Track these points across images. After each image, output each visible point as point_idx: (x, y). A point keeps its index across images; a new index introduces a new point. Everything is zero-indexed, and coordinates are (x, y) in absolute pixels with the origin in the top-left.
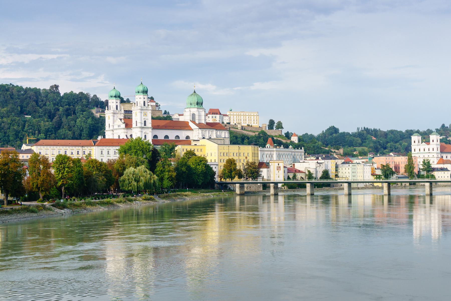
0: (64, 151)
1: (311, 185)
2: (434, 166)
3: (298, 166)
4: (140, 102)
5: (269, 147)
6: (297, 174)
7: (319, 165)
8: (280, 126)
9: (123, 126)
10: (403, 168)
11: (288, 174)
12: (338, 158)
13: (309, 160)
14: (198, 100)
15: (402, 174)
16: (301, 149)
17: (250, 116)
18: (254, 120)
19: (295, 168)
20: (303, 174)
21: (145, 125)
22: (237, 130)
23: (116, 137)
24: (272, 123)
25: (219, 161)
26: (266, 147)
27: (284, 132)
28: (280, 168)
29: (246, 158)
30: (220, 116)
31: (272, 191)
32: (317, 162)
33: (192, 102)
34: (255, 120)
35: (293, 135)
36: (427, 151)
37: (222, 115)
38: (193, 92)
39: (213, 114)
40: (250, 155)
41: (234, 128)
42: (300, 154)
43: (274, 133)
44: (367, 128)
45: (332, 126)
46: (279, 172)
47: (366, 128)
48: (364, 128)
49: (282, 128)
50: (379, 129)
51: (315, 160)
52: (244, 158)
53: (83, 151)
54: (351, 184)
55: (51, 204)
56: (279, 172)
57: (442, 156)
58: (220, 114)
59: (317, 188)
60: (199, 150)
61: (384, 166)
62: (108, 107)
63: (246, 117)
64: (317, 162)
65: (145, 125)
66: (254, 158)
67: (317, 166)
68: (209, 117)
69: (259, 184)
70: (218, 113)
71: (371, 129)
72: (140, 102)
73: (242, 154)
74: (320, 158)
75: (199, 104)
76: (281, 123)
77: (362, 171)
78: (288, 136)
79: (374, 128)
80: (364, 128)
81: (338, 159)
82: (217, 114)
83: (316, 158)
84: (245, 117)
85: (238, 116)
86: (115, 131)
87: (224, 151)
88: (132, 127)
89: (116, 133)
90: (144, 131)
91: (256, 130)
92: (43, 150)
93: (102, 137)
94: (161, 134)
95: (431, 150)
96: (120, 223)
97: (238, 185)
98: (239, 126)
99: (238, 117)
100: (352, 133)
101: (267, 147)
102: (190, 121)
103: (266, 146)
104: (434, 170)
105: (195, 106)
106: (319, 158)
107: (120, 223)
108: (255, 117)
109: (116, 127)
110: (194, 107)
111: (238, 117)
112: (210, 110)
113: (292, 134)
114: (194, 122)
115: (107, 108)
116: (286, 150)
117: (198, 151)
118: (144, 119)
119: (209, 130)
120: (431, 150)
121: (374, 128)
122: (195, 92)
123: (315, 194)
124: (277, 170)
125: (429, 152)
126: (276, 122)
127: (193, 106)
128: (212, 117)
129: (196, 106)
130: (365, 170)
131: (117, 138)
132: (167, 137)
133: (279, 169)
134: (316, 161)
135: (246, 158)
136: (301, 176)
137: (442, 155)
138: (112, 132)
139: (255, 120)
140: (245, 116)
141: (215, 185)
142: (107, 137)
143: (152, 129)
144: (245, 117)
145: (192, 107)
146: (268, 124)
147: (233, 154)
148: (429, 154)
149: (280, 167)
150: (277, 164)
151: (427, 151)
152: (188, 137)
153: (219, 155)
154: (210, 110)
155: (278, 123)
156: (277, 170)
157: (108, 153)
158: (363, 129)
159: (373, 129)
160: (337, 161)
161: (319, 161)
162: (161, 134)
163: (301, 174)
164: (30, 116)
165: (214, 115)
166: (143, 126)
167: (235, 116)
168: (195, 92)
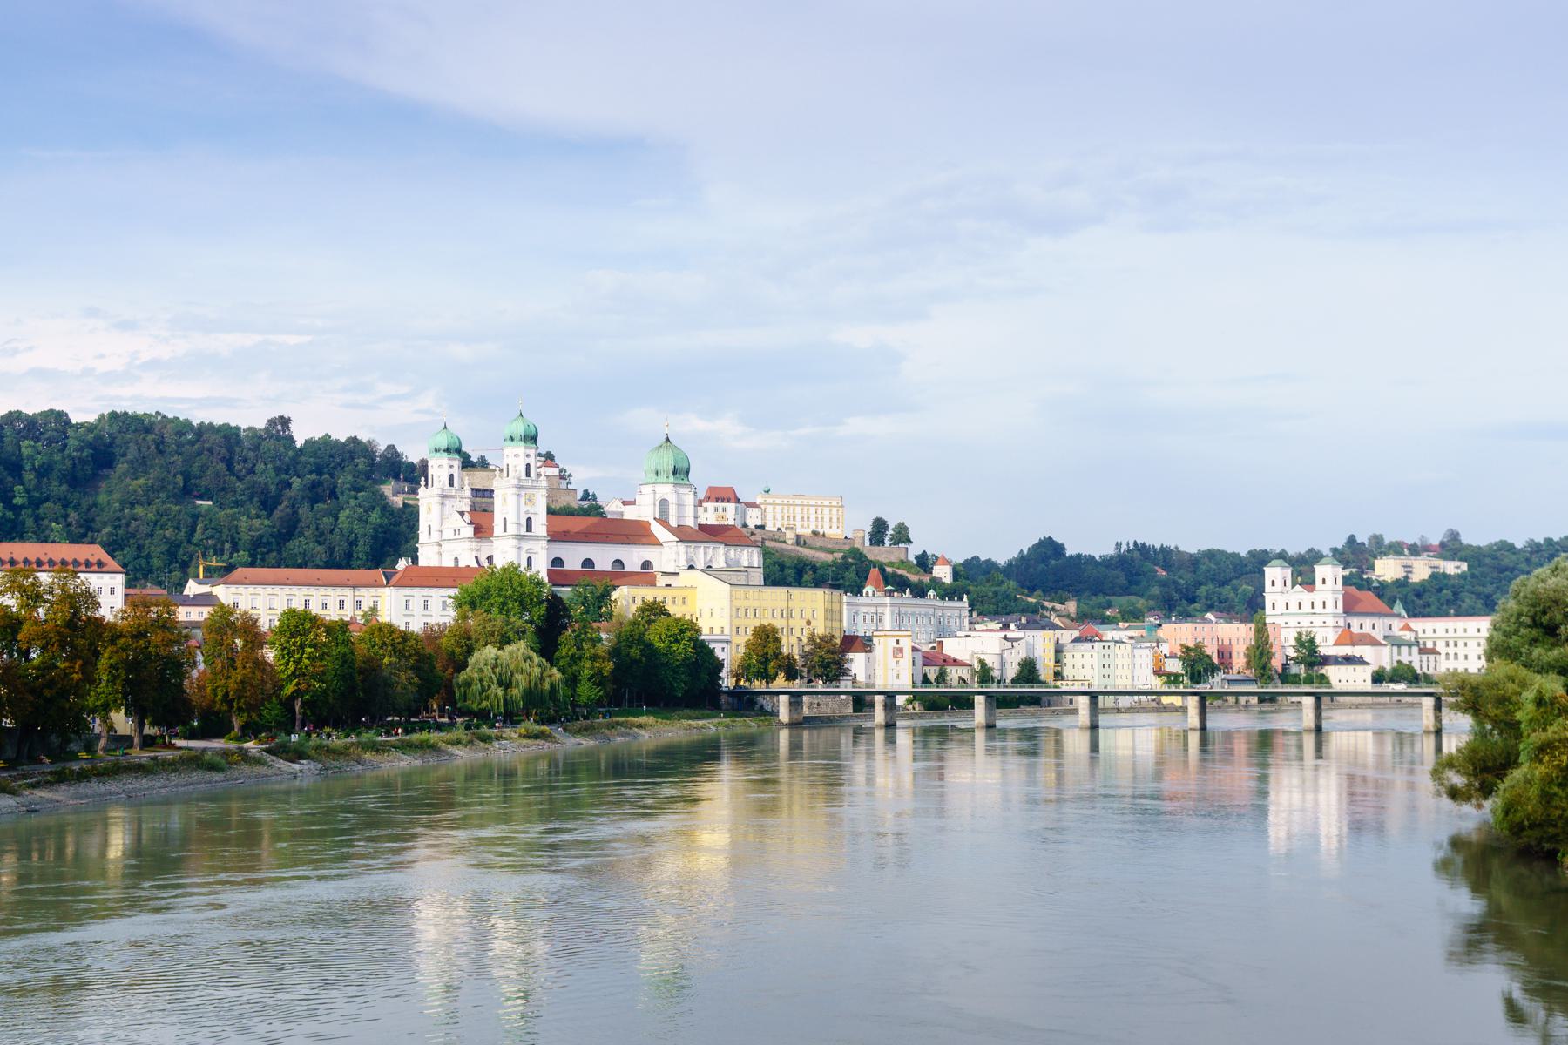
0: (304, 598)
1: (986, 701)
2: (1326, 649)
3: (952, 648)
5: (870, 594)
6: (949, 669)
7: (1009, 644)
8: (902, 536)
10: (1242, 655)
11: (925, 668)
12: (1061, 625)
13: (983, 631)
14: (676, 461)
15: (1239, 673)
16: (961, 599)
18: (831, 519)
20: (965, 669)
21: (529, 528)
22: (784, 546)
24: (879, 527)
27: (913, 552)
28: (902, 653)
29: (809, 623)
30: (736, 508)
31: (879, 715)
32: (1006, 636)
34: (835, 520)
35: (940, 561)
36: (1306, 608)
38: (664, 439)
39: (717, 500)
40: (820, 614)
41: (775, 540)
42: (957, 613)
43: (885, 554)
44: (1143, 545)
45: (1047, 537)
46: (898, 662)
47: (1139, 543)
48: (1135, 543)
49: (909, 541)
50: (1177, 548)
51: (998, 631)
52: (804, 623)
53: (356, 599)
54: (1097, 697)
56: (898, 662)
57: (1349, 624)
58: (738, 501)
59: (952, 709)
60: (679, 601)
61: (1188, 649)
62: (426, 480)
63: (808, 510)
64: (1006, 636)
65: (529, 528)
68: (706, 510)
69: (843, 697)
70: (732, 497)
71: (1154, 546)
73: (796, 613)
74: (1012, 626)
75: (680, 474)
76: (906, 529)
77: (1127, 661)
78: (924, 562)
79: (1162, 545)
80: (1135, 543)
81: (1061, 628)
83: (1001, 625)
85: (786, 507)
86: (445, 546)
87: (746, 604)
90: (526, 545)
94: (573, 555)
95: (1318, 608)
97: (784, 699)
98: (790, 536)
99: (786, 511)
100: (1101, 557)
101: (867, 593)
104: (1326, 660)
108: (834, 510)
109: (448, 534)
110: (665, 480)
111: (786, 511)
112: (711, 489)
113: (936, 560)
114: (663, 522)
115: (423, 483)
116: (919, 601)
117: (674, 602)
118: (527, 512)
120: (1318, 608)
121: (1162, 545)
124: (895, 657)
125: (1313, 611)
126: (892, 524)
127: (662, 478)
128: (716, 510)
129: (672, 479)
130: (1138, 661)
131: (452, 564)
132: (588, 563)
133: (900, 655)
134: (1002, 634)
135: (809, 623)
136: (960, 674)
137: (1349, 620)
138: (436, 548)
139: (835, 520)
142: (422, 562)
143: (548, 541)
145: (658, 481)
148: (1312, 618)
149: (901, 650)
151: (1306, 608)
152: (647, 565)
153: (734, 613)
156: (895, 657)
157: (426, 608)
158: (1131, 547)
159: (1158, 546)
160: (1058, 633)
161: (1010, 635)
162: (573, 555)
163: (960, 669)
164: (210, 503)
165: (720, 505)
166: (523, 531)
167: (779, 508)
168: (668, 440)
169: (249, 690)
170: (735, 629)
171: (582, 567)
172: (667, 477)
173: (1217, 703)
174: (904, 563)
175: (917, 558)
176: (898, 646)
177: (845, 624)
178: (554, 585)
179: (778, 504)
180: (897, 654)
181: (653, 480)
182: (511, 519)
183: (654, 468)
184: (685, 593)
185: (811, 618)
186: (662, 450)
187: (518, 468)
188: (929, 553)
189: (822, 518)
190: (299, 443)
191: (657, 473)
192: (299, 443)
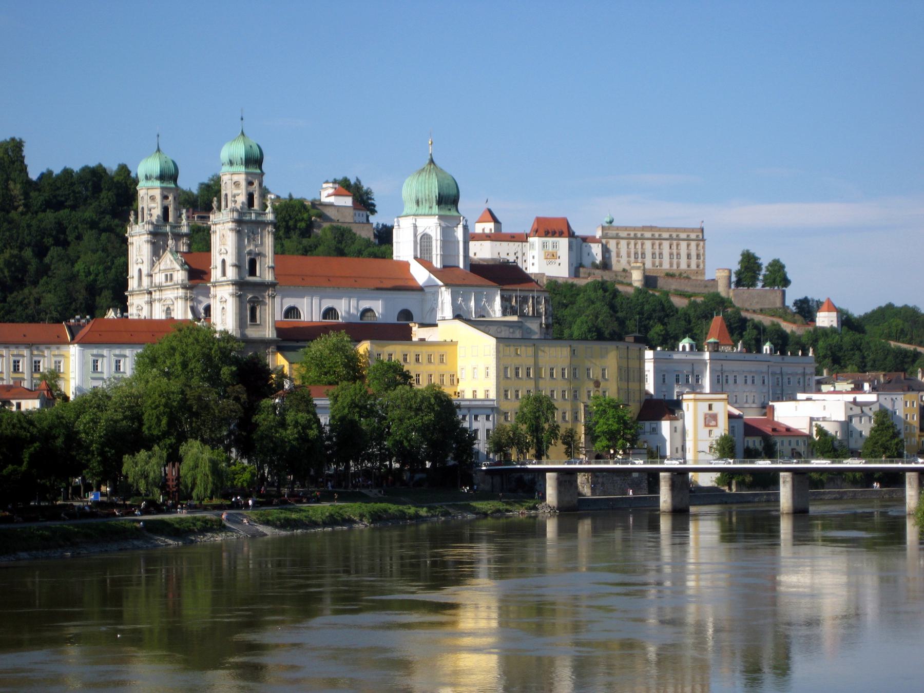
0: (12, 359)
1: (793, 480)
4: (234, 196)
5: (688, 349)
7: (857, 410)
9: (180, 276)
11: (747, 439)
14: (440, 187)
17: (675, 243)
19: (776, 419)
21: (252, 272)
23: (159, 314)
24: (750, 264)
25: (502, 397)
26: (681, 349)
27: (793, 294)
31: (665, 497)
32: (855, 399)
33: (420, 196)
35: (825, 306)
37: (577, 237)
46: (710, 431)
49: (786, 282)
55: (606, 564)
56: (710, 431)
58: (571, 235)
63: (660, 245)
64: (855, 399)
66: (624, 386)
67: (851, 413)
68: (532, 246)
70: (565, 230)
72: (234, 196)
74: (866, 386)
76: (782, 267)
78: (806, 309)
82: (561, 235)
83: (852, 386)
84: (657, 246)
85: (632, 242)
86: (156, 295)
87: (516, 361)
88: (209, 280)
89: (160, 300)
91: (697, 290)
92: (105, 359)
93: (119, 311)
96: (289, 594)
99: (632, 246)
101: (684, 347)
102: (416, 258)
103: (681, 345)
105: (431, 207)
106: (862, 386)
107: (289, 594)
108: (693, 244)
109: (159, 278)
110: (427, 211)
111: (632, 246)
112: (539, 220)
113: (819, 305)
115: (132, 219)
117: (417, 360)
119: (479, 289)
122: (432, 161)
123: (813, 509)
124: (706, 425)
126: (765, 261)
127: (424, 209)
128: (544, 245)
129: (435, 209)
131: (162, 316)
133: (713, 423)
134: (850, 398)
135: (597, 384)
136: (794, 445)
138: (146, 297)
140: (657, 242)
141: (450, 466)
142: (133, 313)
144: (657, 246)
145: (420, 212)
146: (736, 267)
147: (548, 372)
149: (714, 417)
150: (706, 404)
153: (502, 374)
154: (539, 220)
155: (770, 265)
156: (706, 425)
163: (793, 440)
165: (550, 240)
167: (623, 243)
168: (432, 161)
169: (110, 452)
170: (502, 393)
171: (398, 320)
172: (431, 207)
173: (694, 518)
174: (784, 312)
175: (796, 303)
176: (710, 412)
177: (650, 387)
178: (284, 340)
179: (623, 238)
180: (710, 421)
181: (413, 211)
182: (230, 259)
183: (414, 197)
184: (442, 350)
185: (600, 378)
186: (424, 174)
187: (237, 198)
188: (809, 297)
189: (661, 254)
190: (34, 175)
191: (418, 203)
192: (34, 175)
